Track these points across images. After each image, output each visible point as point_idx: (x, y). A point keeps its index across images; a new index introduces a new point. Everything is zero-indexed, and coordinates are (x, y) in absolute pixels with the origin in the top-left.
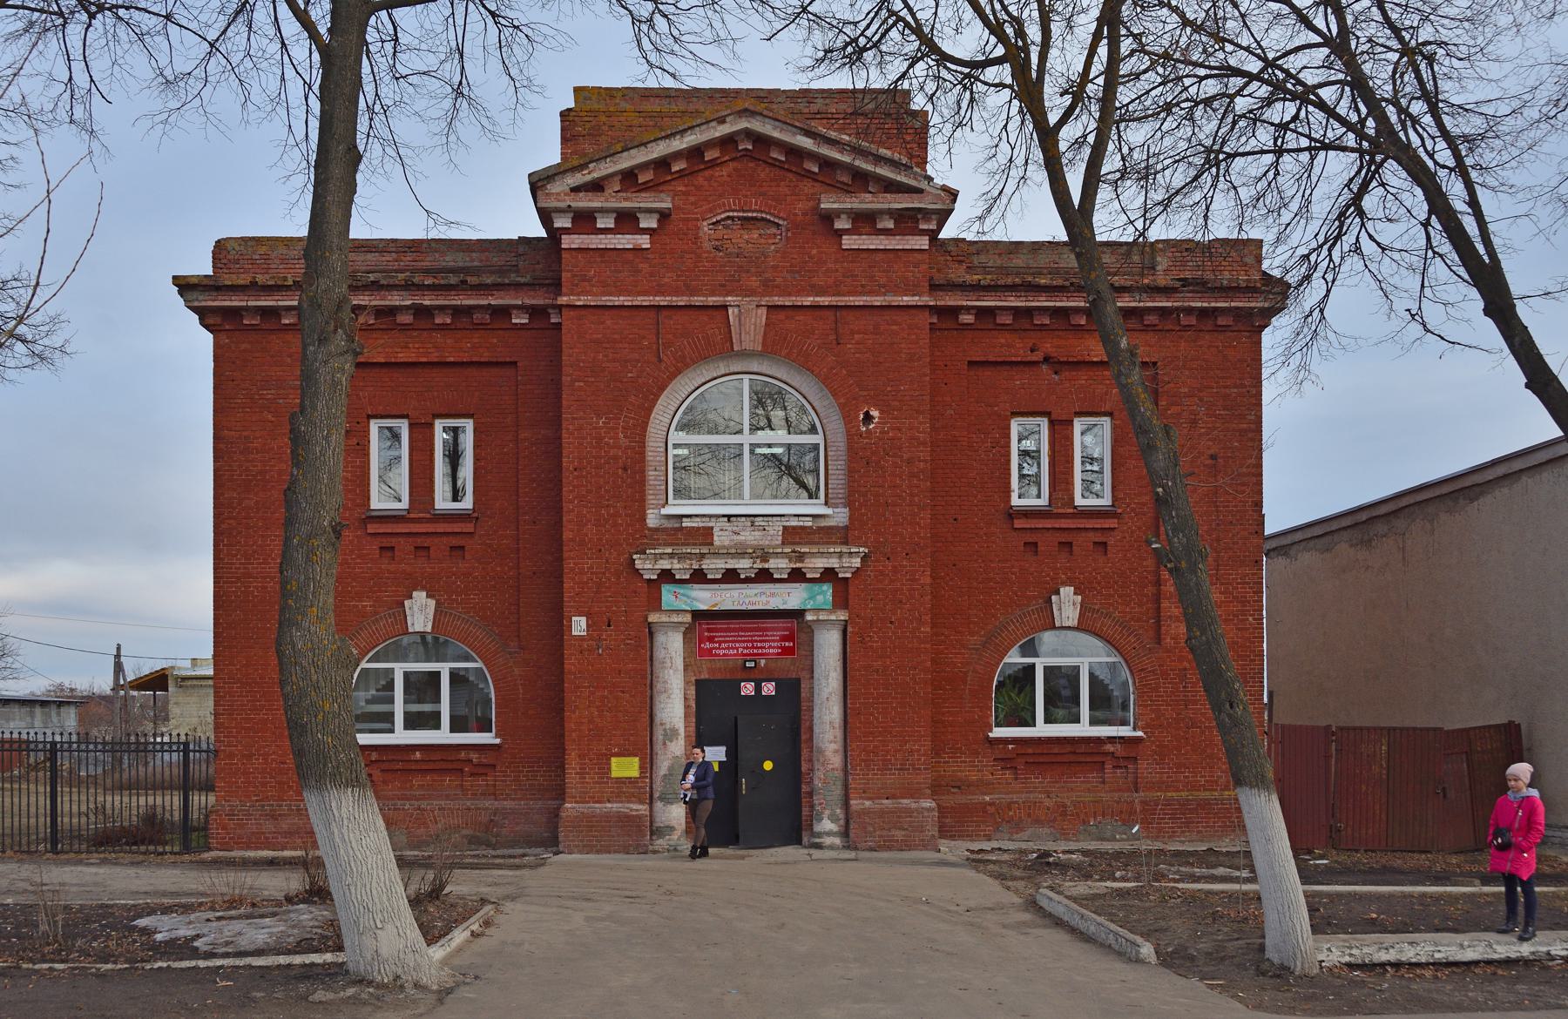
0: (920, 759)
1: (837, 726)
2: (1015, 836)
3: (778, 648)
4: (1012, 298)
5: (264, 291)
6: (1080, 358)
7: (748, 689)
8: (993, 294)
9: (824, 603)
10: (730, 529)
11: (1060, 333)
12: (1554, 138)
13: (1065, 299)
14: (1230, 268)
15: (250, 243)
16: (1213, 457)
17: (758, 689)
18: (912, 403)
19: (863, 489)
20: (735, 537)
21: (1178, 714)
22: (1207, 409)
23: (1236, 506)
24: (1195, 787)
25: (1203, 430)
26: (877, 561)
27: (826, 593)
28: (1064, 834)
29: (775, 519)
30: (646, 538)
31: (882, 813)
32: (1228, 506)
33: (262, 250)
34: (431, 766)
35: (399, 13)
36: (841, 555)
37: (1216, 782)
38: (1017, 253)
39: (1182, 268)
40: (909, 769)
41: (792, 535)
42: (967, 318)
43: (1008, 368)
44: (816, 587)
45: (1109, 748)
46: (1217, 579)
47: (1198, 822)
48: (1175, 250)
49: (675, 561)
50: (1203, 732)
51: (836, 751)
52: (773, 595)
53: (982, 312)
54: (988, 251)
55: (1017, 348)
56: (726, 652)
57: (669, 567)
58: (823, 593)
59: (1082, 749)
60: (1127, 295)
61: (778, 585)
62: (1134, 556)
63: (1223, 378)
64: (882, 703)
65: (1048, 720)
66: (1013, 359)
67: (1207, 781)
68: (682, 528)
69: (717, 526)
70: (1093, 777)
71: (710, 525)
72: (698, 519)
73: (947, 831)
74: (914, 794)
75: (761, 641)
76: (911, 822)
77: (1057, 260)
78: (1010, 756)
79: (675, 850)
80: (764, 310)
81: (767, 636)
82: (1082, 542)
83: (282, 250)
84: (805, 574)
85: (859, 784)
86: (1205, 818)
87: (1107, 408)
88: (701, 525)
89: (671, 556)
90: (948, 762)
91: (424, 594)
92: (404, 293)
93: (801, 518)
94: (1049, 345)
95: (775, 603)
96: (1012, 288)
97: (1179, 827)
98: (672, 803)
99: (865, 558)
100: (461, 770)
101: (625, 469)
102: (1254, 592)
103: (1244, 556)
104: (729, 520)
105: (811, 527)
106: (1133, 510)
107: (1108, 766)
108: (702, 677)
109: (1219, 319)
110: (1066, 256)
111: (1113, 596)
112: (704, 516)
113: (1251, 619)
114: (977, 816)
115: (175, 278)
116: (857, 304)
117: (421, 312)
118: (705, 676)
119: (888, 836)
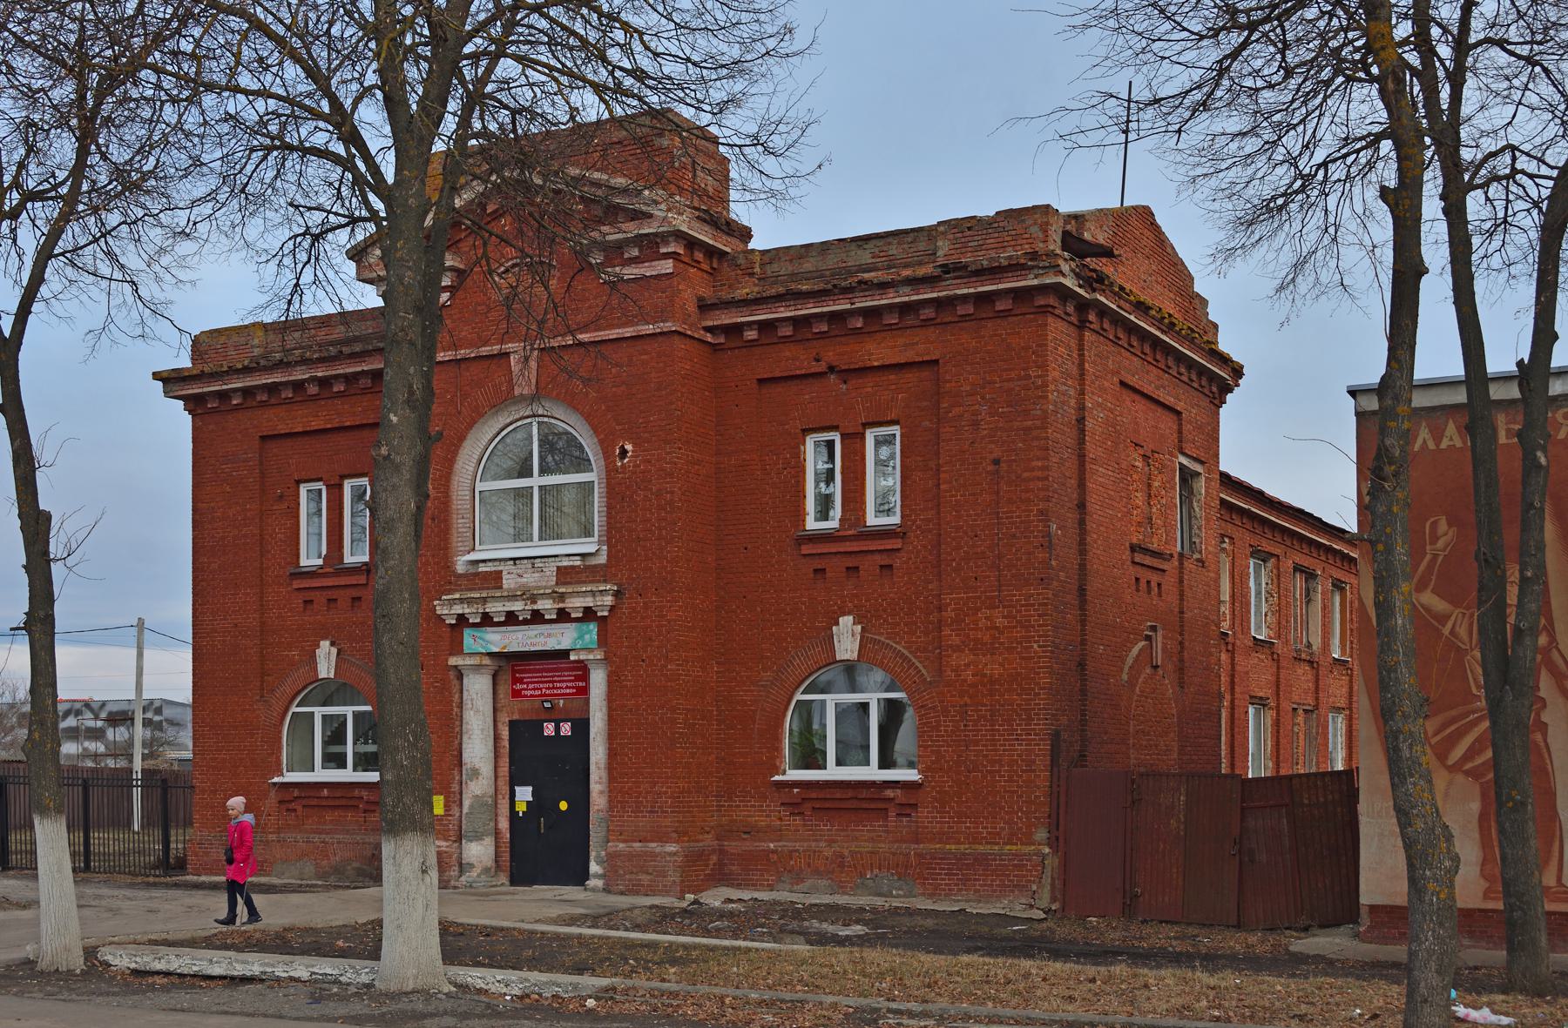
0: (667, 802)
1: (602, 766)
2: (795, 887)
3: (573, 688)
4: (782, 309)
5: (879, 289)
6: (861, 365)
7: (549, 729)
8: (765, 306)
9: (591, 642)
10: (515, 571)
11: (843, 339)
13: (831, 303)
14: (1013, 243)
15: (214, 335)
16: (996, 462)
17: (557, 729)
18: (660, 433)
19: (618, 525)
20: (519, 580)
21: (959, 756)
22: (990, 407)
23: (1019, 517)
24: (975, 839)
25: (985, 432)
26: (631, 598)
27: (592, 631)
28: (842, 887)
29: (550, 559)
30: (447, 580)
31: (631, 856)
32: (1012, 517)
33: (222, 340)
34: (337, 803)
36: (593, 593)
37: (999, 834)
38: (807, 256)
39: (963, 250)
40: (657, 812)
41: (564, 574)
42: (751, 334)
43: (798, 381)
44: (584, 626)
45: (889, 793)
46: (1000, 601)
47: (975, 880)
48: (956, 230)
49: (466, 606)
50: (984, 777)
51: (601, 792)
52: (549, 635)
53: (764, 326)
54: (780, 258)
55: (798, 359)
56: (532, 692)
57: (460, 612)
58: (590, 632)
59: (864, 794)
60: (891, 290)
61: (548, 626)
63: (1006, 370)
64: (634, 744)
65: (839, 763)
66: (798, 372)
67: (988, 833)
68: (477, 574)
69: (505, 568)
70: (879, 826)
71: (500, 568)
72: (490, 564)
73: (734, 879)
74: (662, 838)
75: (560, 682)
76: (655, 866)
77: (845, 259)
78: (796, 801)
79: (471, 886)
81: (564, 676)
82: (869, 565)
83: (235, 338)
84: (492, 618)
85: (617, 826)
86: (983, 875)
87: (893, 416)
88: (493, 569)
89: (461, 601)
90: (739, 806)
92: (304, 367)
93: (572, 558)
94: (831, 354)
95: (552, 644)
96: (779, 298)
97: (956, 885)
98: (471, 841)
99: (617, 594)
100: (357, 807)
101: (433, 519)
102: (1039, 615)
103: (1029, 574)
104: (515, 564)
105: (579, 566)
106: (919, 527)
107: (892, 814)
108: (514, 718)
109: (997, 303)
110: (853, 253)
111: (899, 624)
112: (495, 560)
113: (1035, 646)
114: (761, 865)
115: (154, 374)
116: (611, 337)
117: (324, 382)
118: (516, 717)
119: (636, 880)
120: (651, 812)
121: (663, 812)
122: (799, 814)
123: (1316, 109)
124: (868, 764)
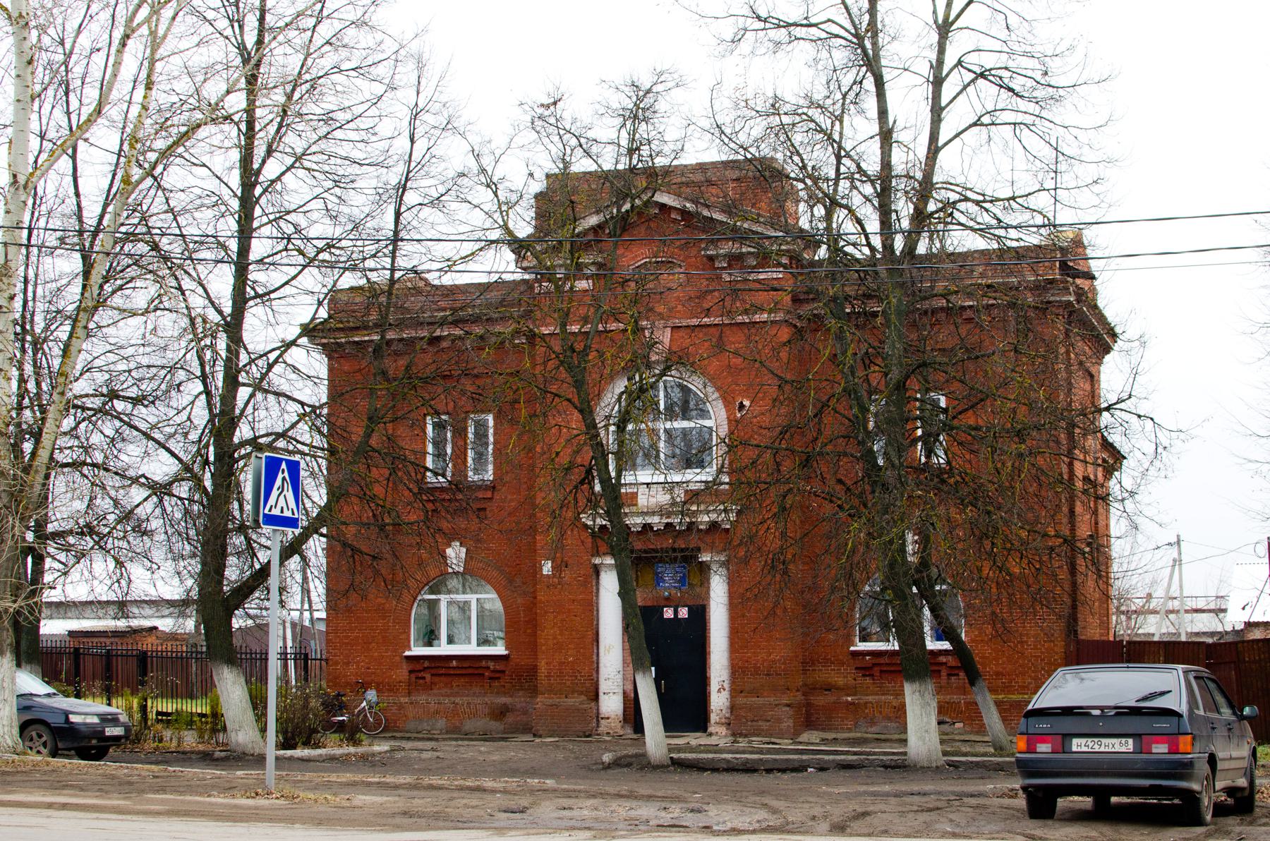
7: (669, 613)
12: (379, 9)
17: (676, 613)
35: (935, 181)
41: (693, 496)
45: (943, 659)
62: (819, 541)
80: (669, 329)
91: (458, 544)
100: (483, 675)
107: (944, 673)
120: (768, 675)
121: (777, 674)
122: (869, 675)
123: (982, 207)
124: (470, 643)
